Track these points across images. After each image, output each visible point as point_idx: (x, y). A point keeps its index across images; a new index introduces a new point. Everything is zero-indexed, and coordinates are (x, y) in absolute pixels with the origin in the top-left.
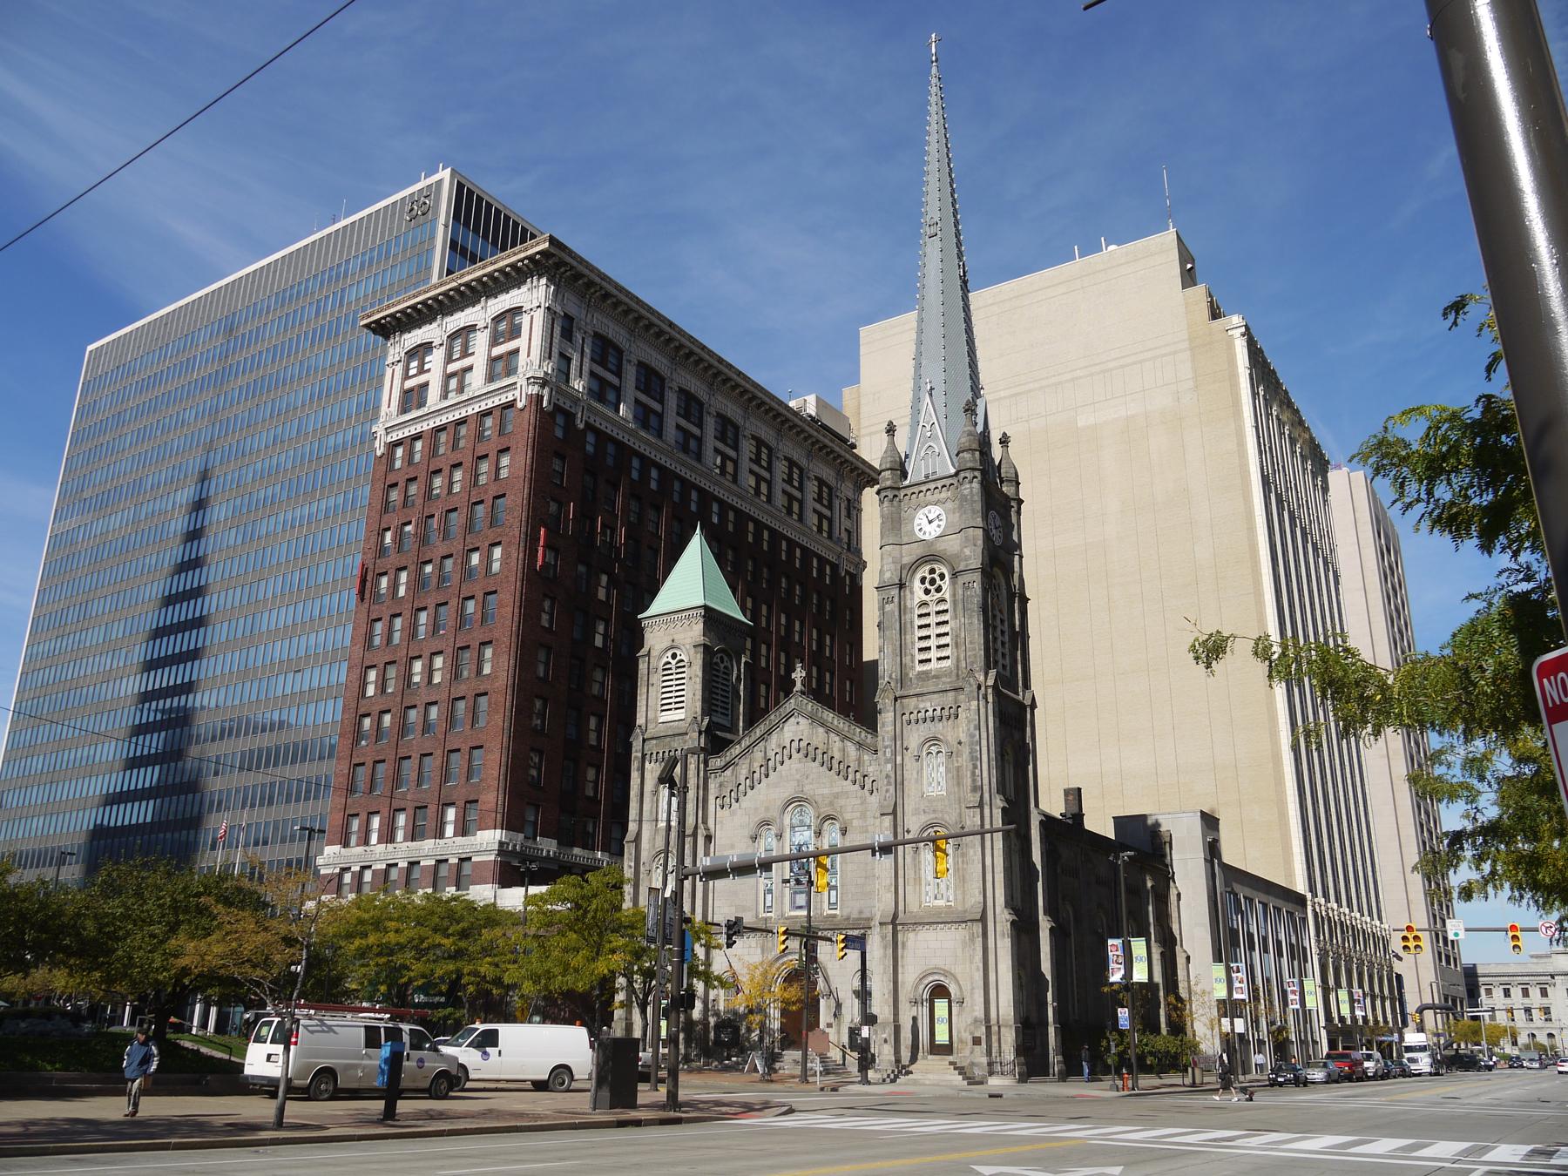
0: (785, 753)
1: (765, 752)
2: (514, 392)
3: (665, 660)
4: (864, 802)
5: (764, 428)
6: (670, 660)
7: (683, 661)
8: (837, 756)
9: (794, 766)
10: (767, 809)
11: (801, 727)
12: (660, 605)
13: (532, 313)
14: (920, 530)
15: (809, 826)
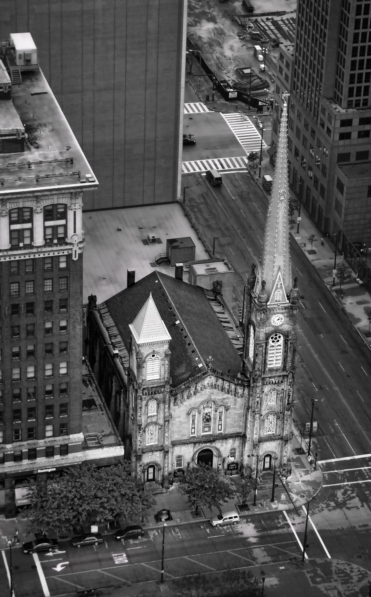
1: (196, 388)
3: (149, 357)
6: (151, 357)
8: (227, 387)
9: (208, 391)
11: (212, 379)
15: (211, 407)
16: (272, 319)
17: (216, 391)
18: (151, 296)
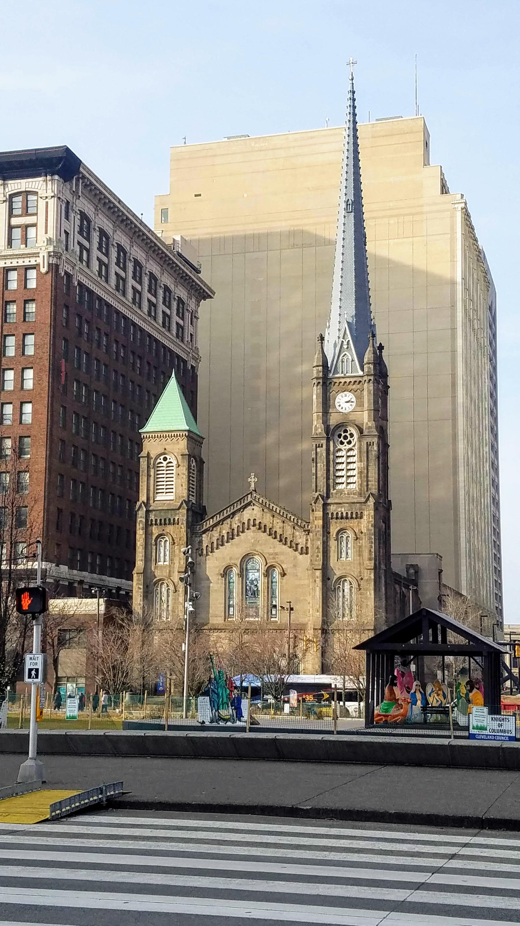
0: (243, 528)
1: (231, 525)
2: (37, 259)
4: (295, 558)
5: (155, 266)
6: (162, 461)
7: (172, 462)
8: (279, 532)
10: (231, 559)
11: (255, 512)
12: (152, 425)
13: (47, 200)
14: (339, 406)
15: (258, 570)
16: (337, 400)
17: (264, 536)
18: (173, 375)
